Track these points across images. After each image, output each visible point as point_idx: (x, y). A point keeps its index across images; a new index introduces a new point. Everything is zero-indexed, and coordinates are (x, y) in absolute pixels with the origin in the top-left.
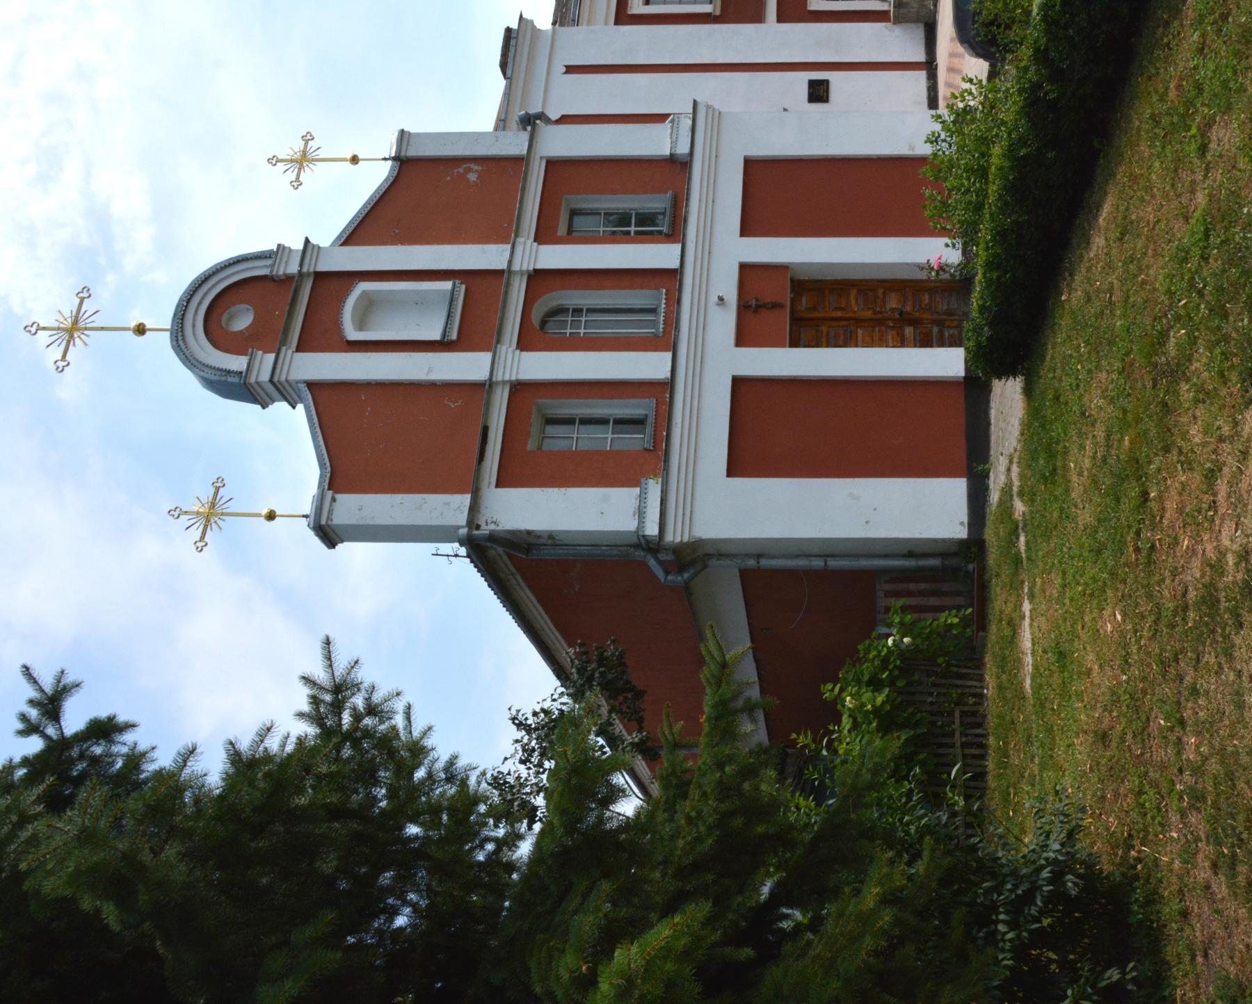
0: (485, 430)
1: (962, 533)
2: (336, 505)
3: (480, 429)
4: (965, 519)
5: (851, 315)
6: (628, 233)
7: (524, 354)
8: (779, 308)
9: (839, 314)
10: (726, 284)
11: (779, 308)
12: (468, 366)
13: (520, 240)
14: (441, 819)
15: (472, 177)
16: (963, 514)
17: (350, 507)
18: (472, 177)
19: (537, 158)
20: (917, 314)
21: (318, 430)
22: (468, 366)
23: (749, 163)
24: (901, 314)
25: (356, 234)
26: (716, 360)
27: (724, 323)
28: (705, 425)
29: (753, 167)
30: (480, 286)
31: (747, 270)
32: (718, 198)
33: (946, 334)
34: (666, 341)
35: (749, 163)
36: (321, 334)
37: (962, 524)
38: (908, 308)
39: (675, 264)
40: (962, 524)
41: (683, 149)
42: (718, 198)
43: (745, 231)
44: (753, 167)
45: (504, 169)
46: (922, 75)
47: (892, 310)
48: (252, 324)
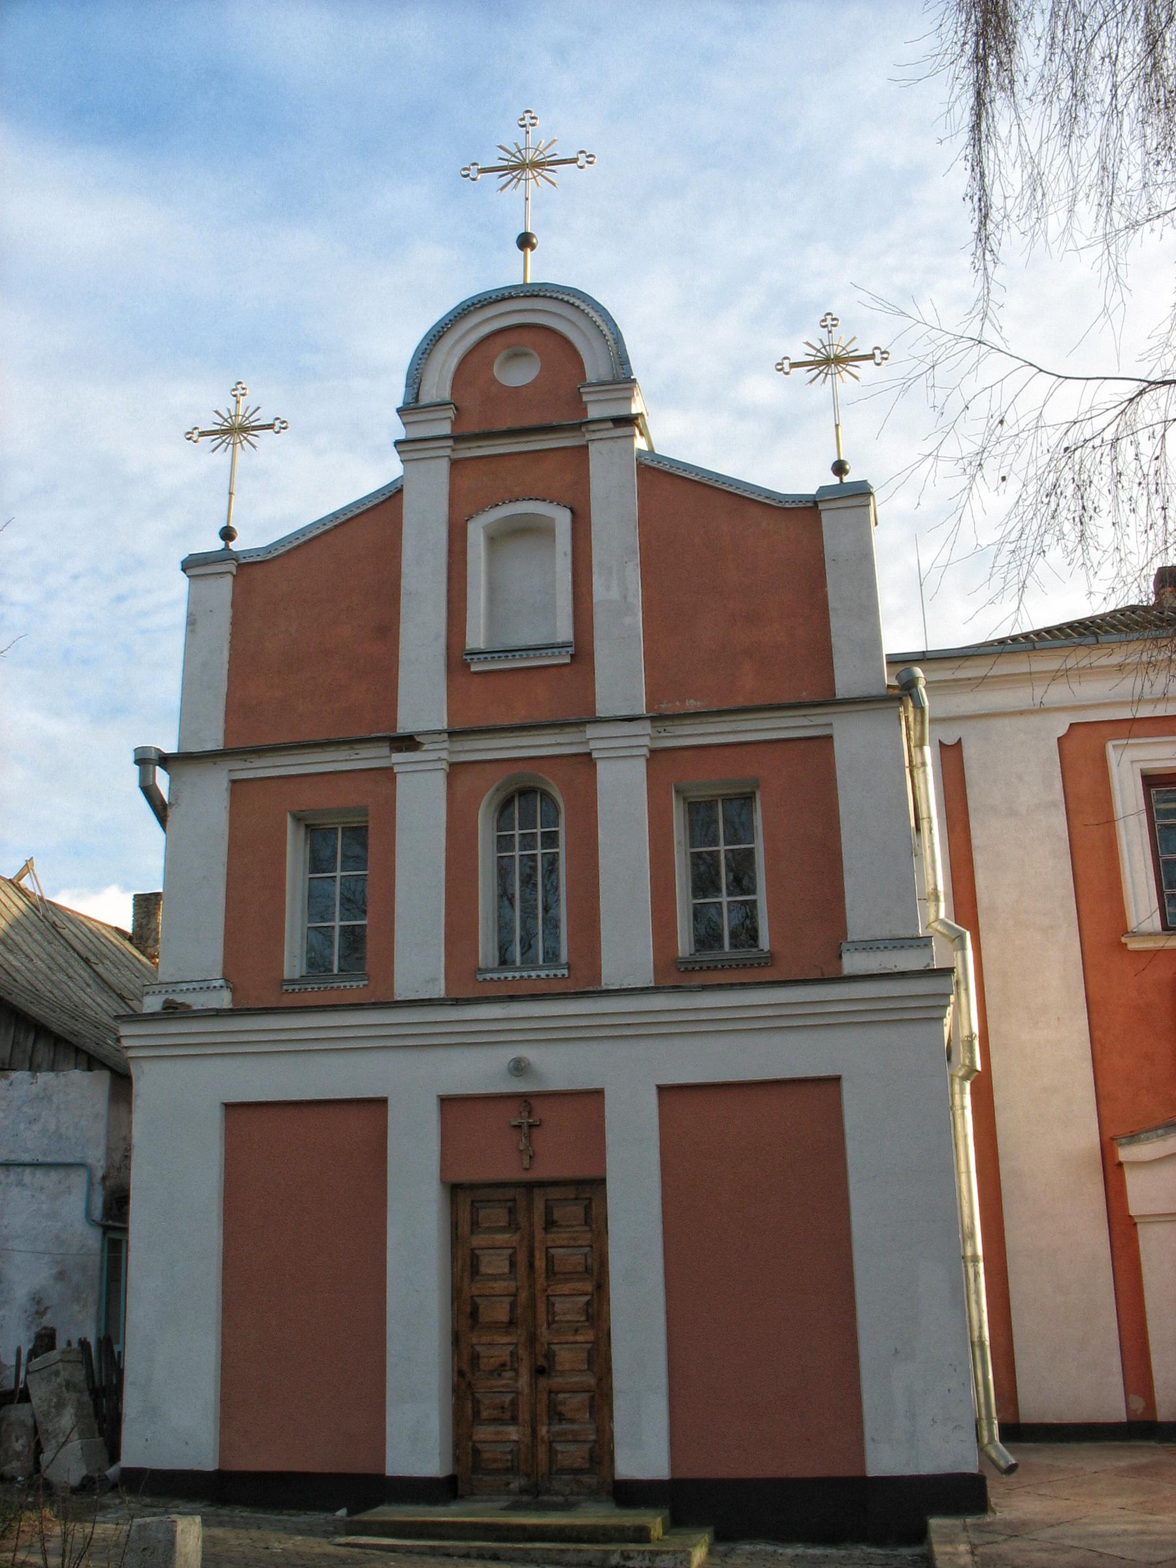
7: (641, 765)
10: (559, 1068)
12: (422, 700)
13: (646, 728)
17: (222, 589)
22: (422, 700)
26: (629, 1065)
27: (479, 1071)
29: (818, 1097)
32: (747, 1042)
39: (610, 977)
42: (747, 1042)
44: (818, 1097)
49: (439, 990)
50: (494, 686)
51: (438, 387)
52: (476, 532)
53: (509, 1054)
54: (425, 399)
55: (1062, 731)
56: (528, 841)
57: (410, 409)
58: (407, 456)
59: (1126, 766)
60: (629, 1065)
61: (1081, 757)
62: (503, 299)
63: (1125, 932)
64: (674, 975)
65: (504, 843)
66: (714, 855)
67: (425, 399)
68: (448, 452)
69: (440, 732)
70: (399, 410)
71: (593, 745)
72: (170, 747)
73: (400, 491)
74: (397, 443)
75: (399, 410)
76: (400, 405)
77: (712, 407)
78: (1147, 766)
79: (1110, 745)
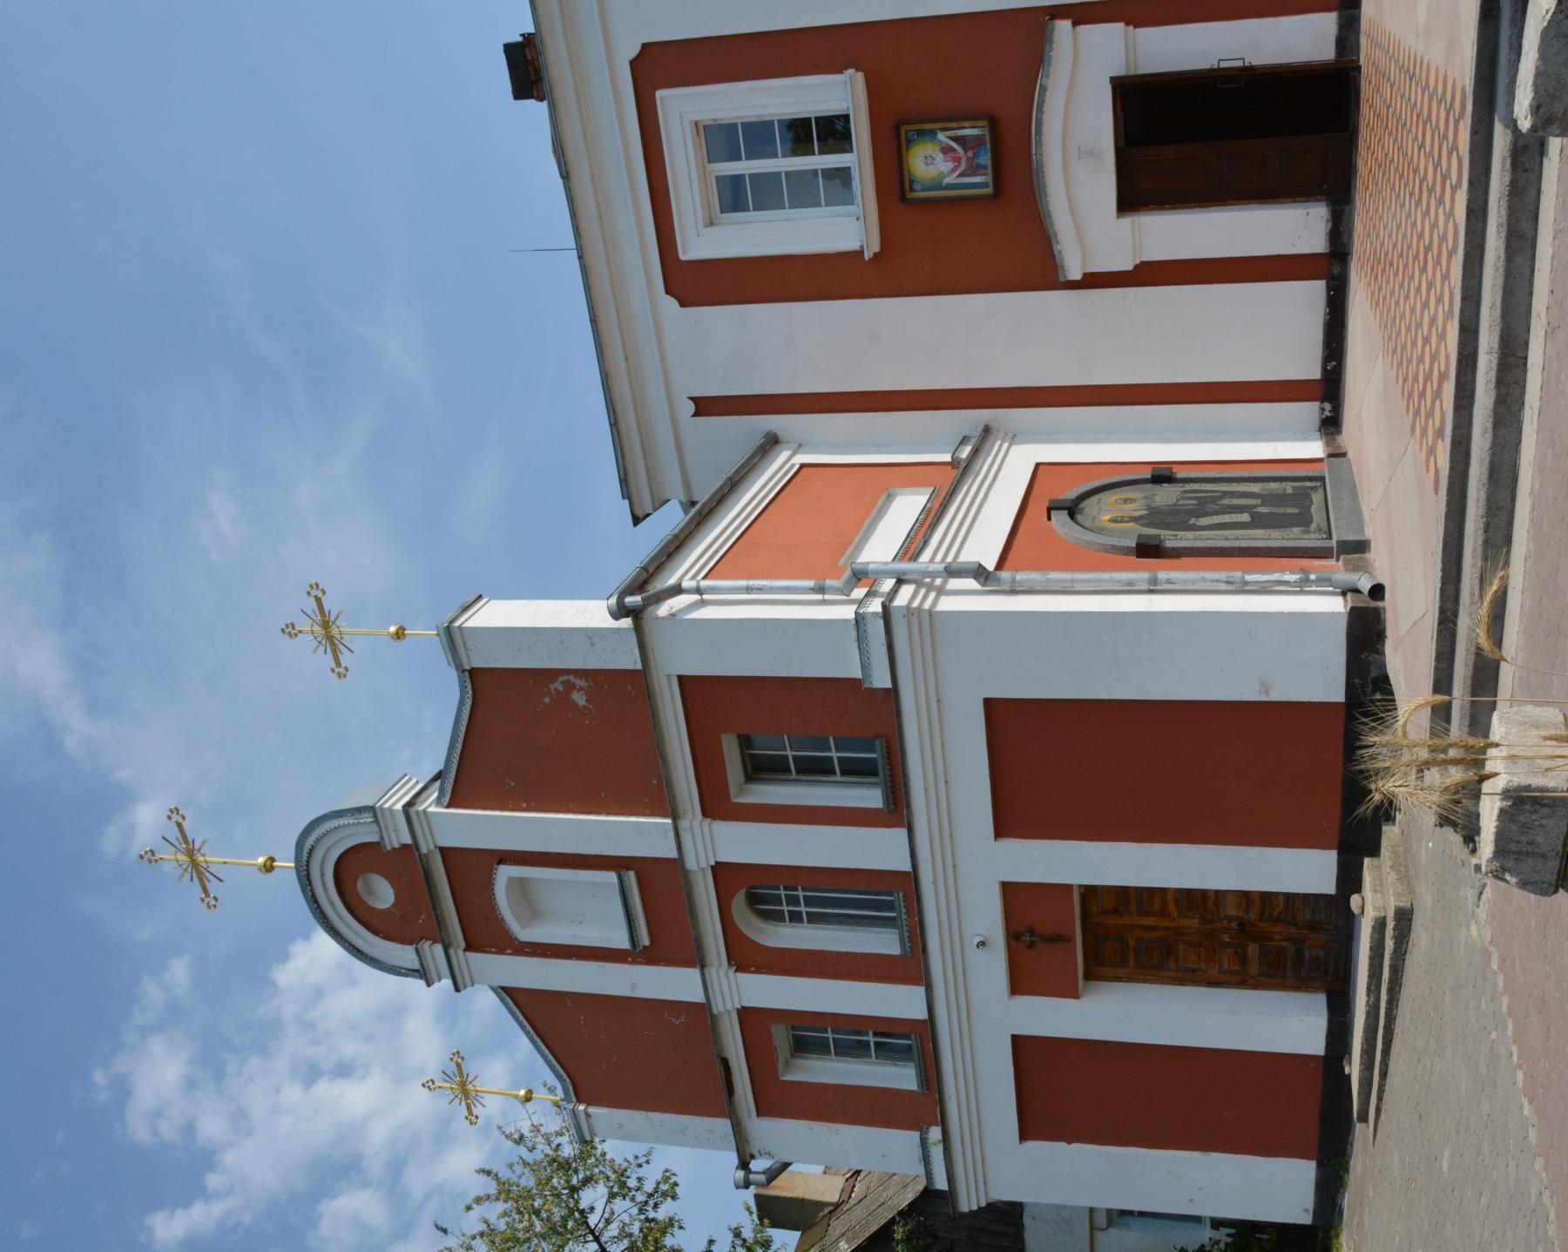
0: (725, 1063)
1: (1307, 1220)
2: (594, 1121)
3: (718, 1062)
4: (1311, 1207)
5: (1166, 923)
6: (876, 1034)
8: (1061, 938)
9: (1151, 921)
10: (988, 919)
11: (1061, 938)
14: (575, 704)
15: (580, 699)
16: (1308, 1200)
18: (580, 699)
19: (664, 683)
20: (1265, 926)
21: (536, 1038)
23: (994, 708)
24: (1241, 925)
25: (468, 779)
27: (992, 968)
28: (985, 1088)
30: (656, 886)
31: (1012, 893)
32: (952, 764)
33: (1307, 956)
34: (910, 966)
35: (994, 708)
36: (486, 934)
37: (1307, 1211)
38: (1253, 916)
40: (1307, 1211)
41: (881, 680)
42: (952, 764)
43: (1005, 826)
45: (624, 691)
46: (1316, 290)
47: (1230, 919)
48: (384, 876)
49: (921, 990)
50: (664, 931)
51: (404, 955)
52: (525, 934)
53: (973, 953)
54: (417, 966)
55: (673, 302)
56: (793, 900)
57: (423, 973)
58: (468, 981)
59: (702, 242)
60: (973, 864)
61: (696, 283)
62: (316, 901)
63: (861, 253)
64: (897, 811)
65: (796, 918)
66: (781, 904)
67: (417, 966)
68: (460, 952)
69: (703, 975)
70: (429, 985)
71: (704, 865)
72: (733, 1159)
73: (503, 988)
74: (457, 989)
75: (429, 985)
76: (423, 982)
77: (396, 760)
78: (701, 223)
79: (683, 257)
